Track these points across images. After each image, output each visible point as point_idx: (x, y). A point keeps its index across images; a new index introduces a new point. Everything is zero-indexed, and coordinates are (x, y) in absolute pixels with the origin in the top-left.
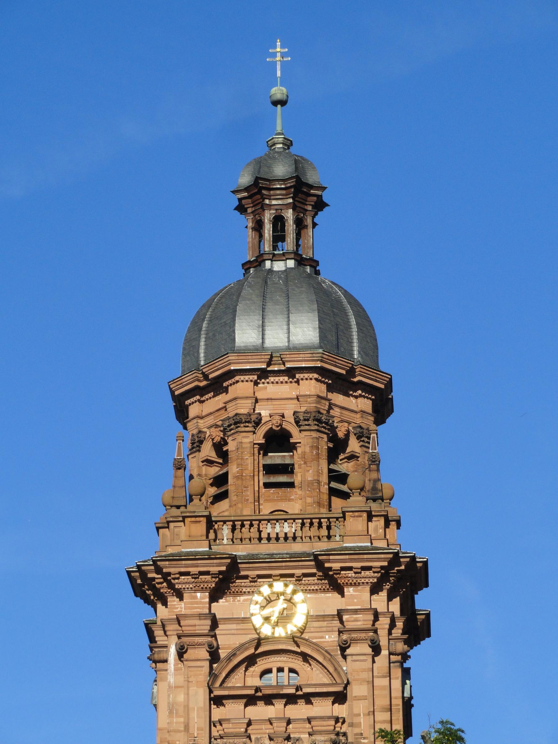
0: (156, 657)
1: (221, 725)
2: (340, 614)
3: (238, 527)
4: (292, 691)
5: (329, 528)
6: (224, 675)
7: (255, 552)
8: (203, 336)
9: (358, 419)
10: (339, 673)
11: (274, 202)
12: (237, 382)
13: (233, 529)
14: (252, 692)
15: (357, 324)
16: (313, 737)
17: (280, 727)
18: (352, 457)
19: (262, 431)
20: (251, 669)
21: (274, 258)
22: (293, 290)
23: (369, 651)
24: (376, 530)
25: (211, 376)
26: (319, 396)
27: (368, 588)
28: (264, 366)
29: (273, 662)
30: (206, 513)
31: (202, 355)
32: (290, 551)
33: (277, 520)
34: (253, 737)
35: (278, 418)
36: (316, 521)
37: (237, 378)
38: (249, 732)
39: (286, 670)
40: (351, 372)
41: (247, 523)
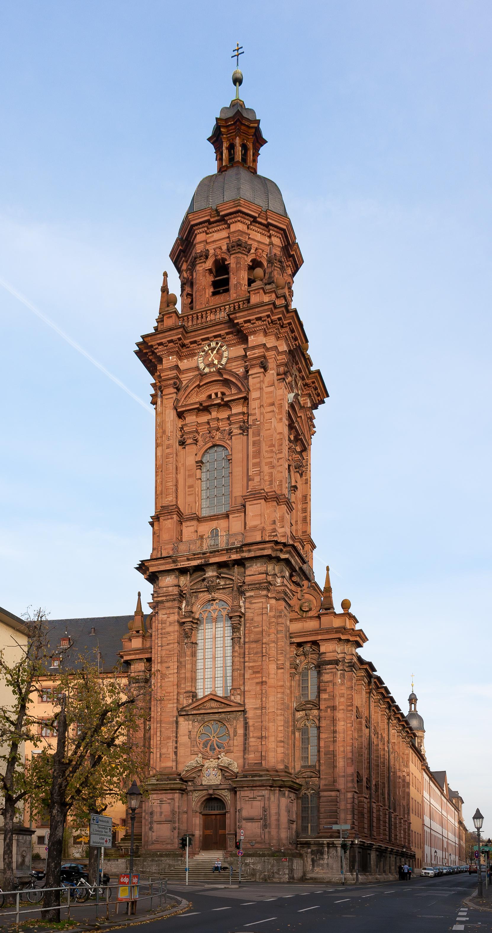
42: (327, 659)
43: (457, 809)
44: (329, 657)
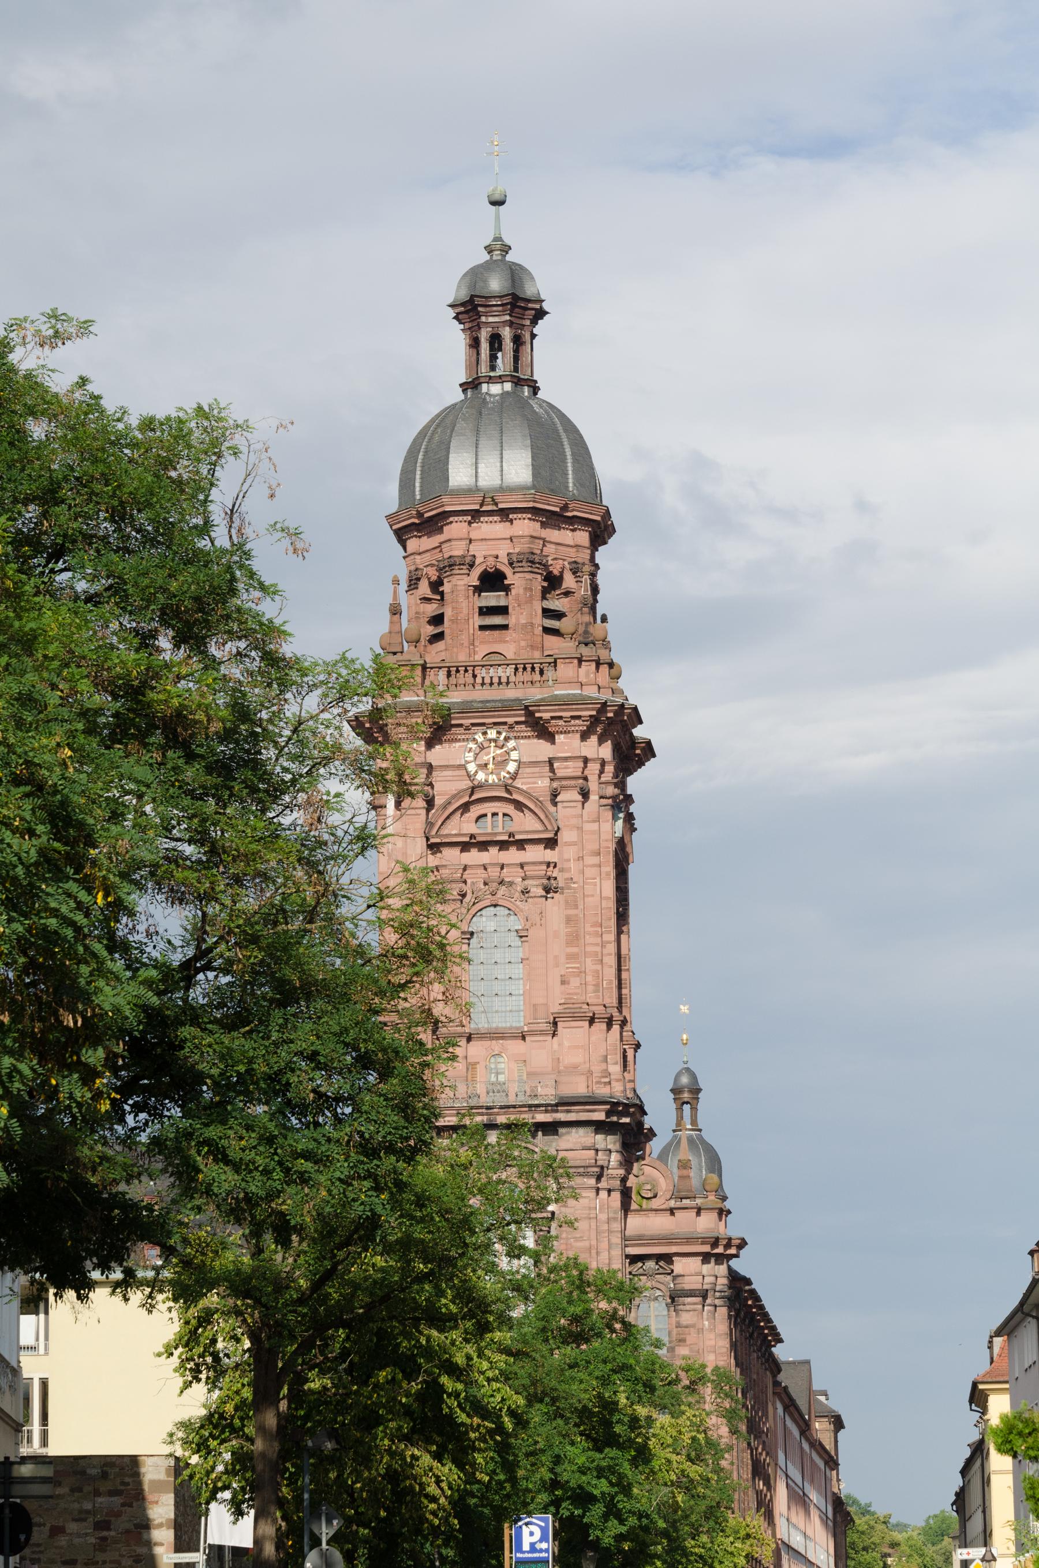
0: (377, 803)
1: (438, 871)
2: (550, 762)
3: (453, 673)
4: (506, 838)
5: (542, 672)
6: (440, 823)
7: (470, 699)
8: (419, 469)
9: (572, 553)
10: (549, 820)
11: (491, 319)
12: (451, 522)
13: (449, 675)
14: (467, 839)
15: (573, 454)
16: (526, 882)
17: (494, 872)
18: (567, 594)
19: (477, 572)
20: (467, 815)
21: (490, 380)
22: (507, 423)
23: (580, 798)
24: (587, 674)
25: (426, 515)
26: (532, 537)
27: (578, 735)
28: (477, 507)
29: (488, 808)
30: (422, 662)
31: (418, 489)
32: (503, 698)
33: (491, 666)
34: (469, 881)
35: (492, 559)
36: (529, 666)
37: (451, 519)
38: (464, 877)
39: (500, 815)
40: (565, 508)
41: (462, 669)
42: (687, 1287)
43: (636, 1051)
44: (691, 1283)
